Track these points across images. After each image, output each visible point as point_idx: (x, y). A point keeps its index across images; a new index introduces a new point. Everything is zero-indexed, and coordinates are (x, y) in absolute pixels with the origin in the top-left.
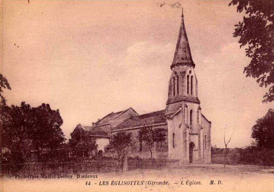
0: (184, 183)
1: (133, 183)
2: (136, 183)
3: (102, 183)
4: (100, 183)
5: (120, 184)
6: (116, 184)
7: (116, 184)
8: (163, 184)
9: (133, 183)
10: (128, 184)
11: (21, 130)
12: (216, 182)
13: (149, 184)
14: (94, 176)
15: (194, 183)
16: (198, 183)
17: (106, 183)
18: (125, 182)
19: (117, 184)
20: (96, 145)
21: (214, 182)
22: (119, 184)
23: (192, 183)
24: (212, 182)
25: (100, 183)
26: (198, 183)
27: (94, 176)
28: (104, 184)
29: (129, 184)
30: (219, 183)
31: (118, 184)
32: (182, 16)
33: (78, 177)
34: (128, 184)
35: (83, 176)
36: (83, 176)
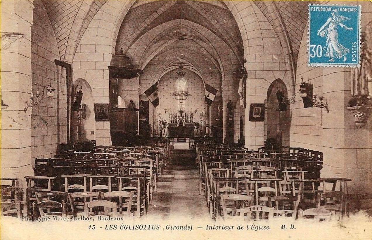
0: (250, 227)
1: (147, 227)
2: (151, 227)
3: (108, 227)
4: (106, 227)
5: (107, 229)
6: (127, 229)
7: (126, 228)
8: (185, 228)
9: (147, 227)
10: (141, 228)
11: (119, 51)
12: (288, 227)
13: (167, 228)
14: (119, 219)
15: (261, 227)
16: (266, 227)
17: (113, 227)
18: (137, 226)
19: (127, 228)
20: (362, 50)
21: (285, 226)
22: (129, 229)
23: (259, 227)
24: (283, 227)
25: (106, 227)
26: (266, 227)
27: (119, 219)
28: (111, 228)
29: (179, 228)
30: (292, 227)
31: (128, 228)
32: (303, 78)
33: (99, 219)
34: (141, 228)
35: (106, 218)
36: (106, 218)
